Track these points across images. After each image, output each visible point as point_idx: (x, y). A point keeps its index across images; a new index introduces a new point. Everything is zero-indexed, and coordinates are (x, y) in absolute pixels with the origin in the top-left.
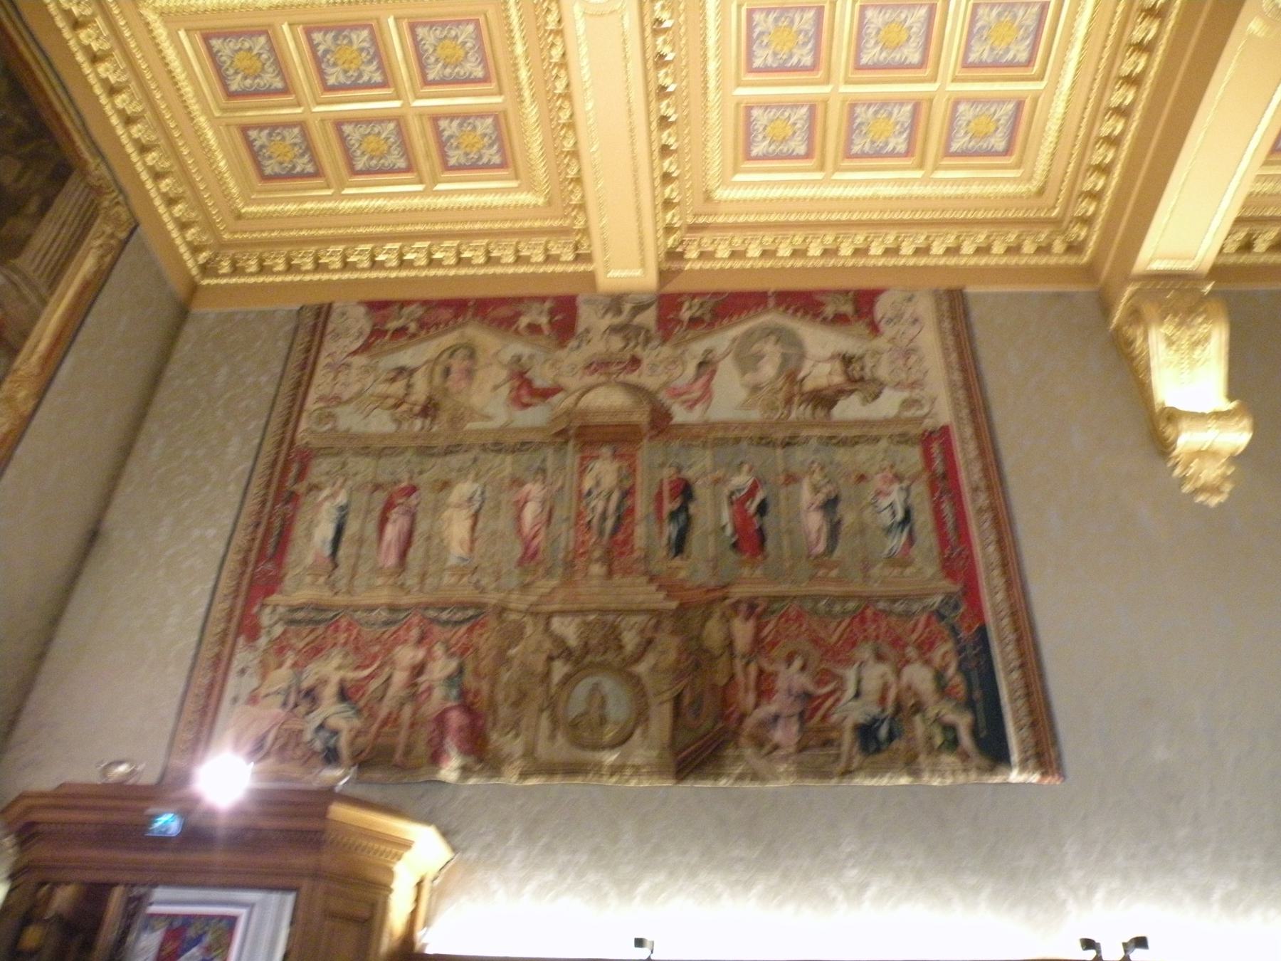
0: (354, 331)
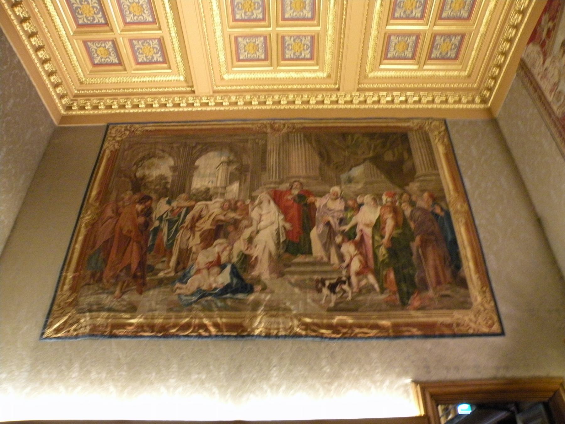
0: (536, 56)
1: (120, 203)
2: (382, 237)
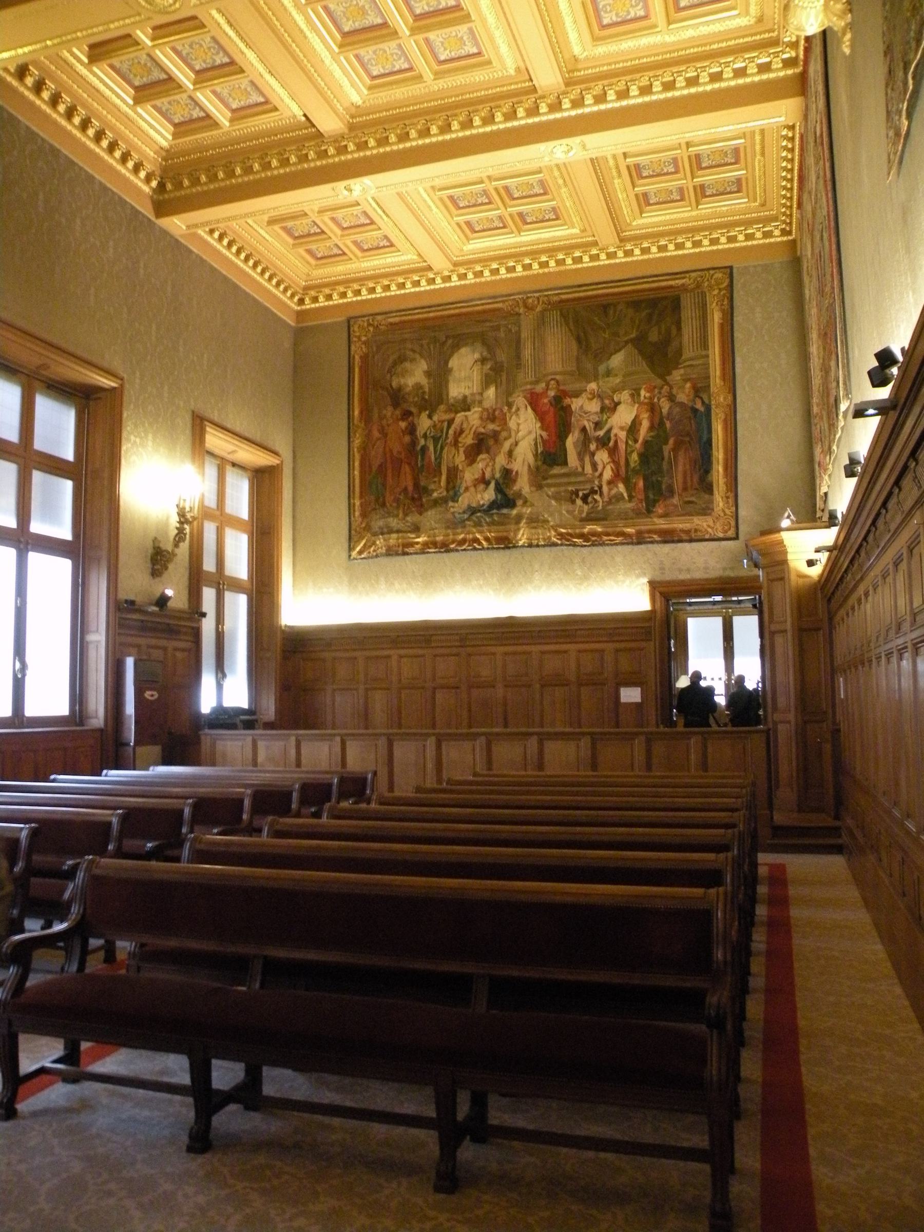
1: (384, 422)
2: (636, 441)
